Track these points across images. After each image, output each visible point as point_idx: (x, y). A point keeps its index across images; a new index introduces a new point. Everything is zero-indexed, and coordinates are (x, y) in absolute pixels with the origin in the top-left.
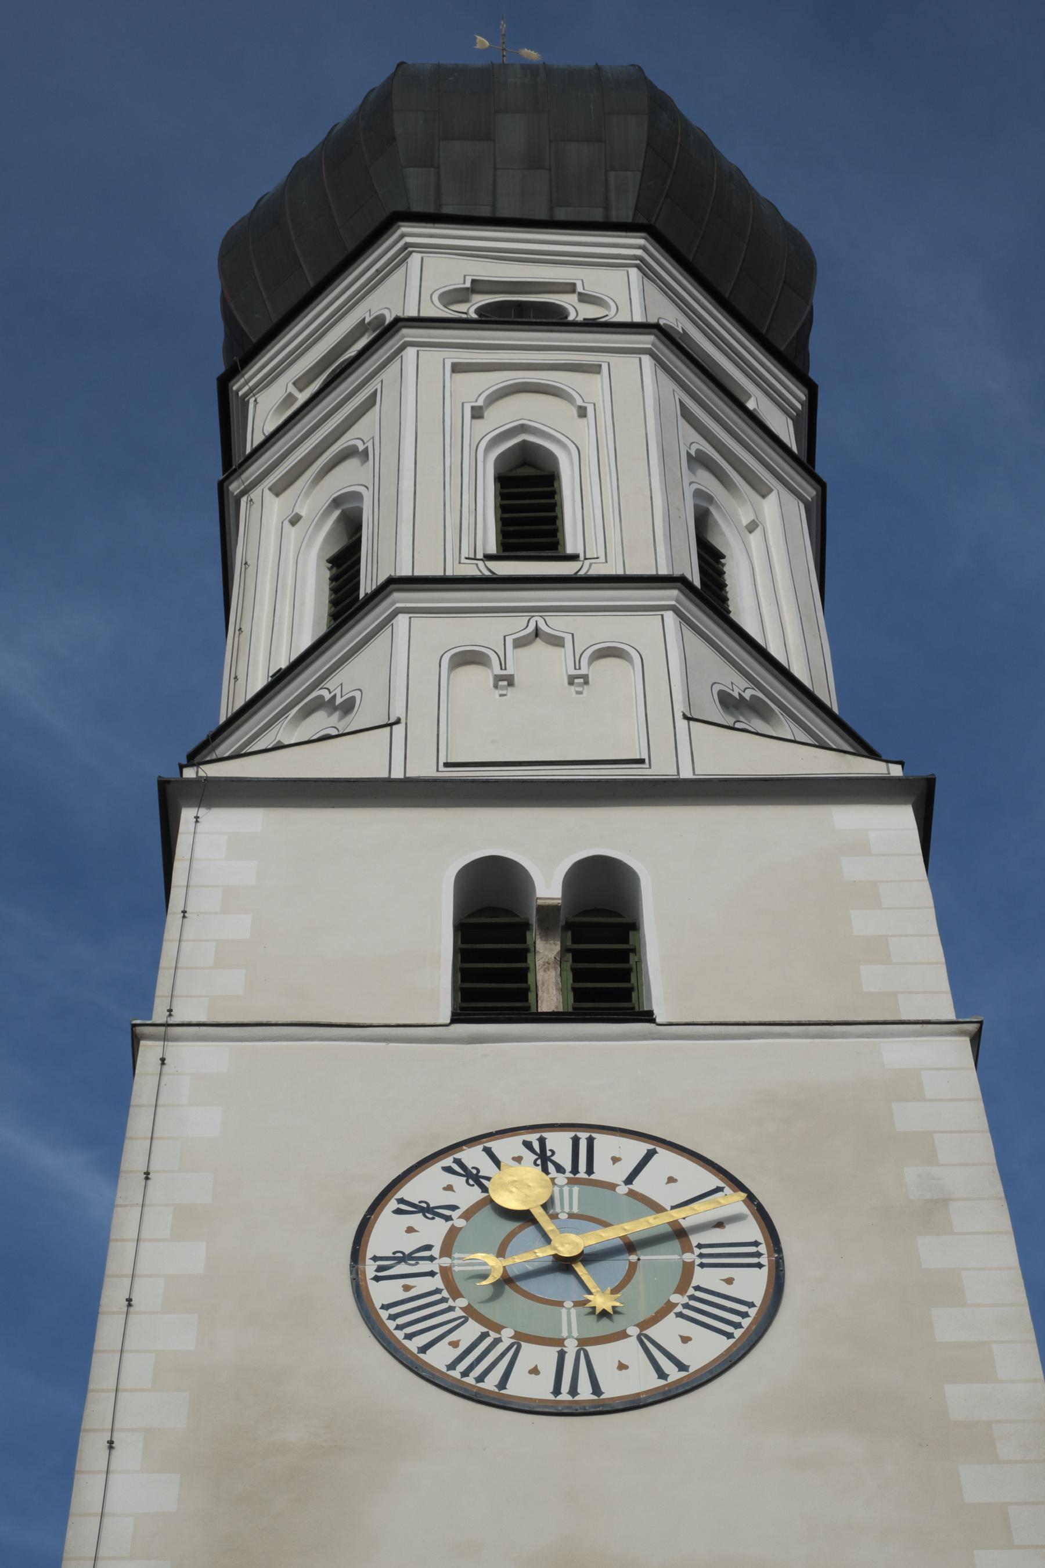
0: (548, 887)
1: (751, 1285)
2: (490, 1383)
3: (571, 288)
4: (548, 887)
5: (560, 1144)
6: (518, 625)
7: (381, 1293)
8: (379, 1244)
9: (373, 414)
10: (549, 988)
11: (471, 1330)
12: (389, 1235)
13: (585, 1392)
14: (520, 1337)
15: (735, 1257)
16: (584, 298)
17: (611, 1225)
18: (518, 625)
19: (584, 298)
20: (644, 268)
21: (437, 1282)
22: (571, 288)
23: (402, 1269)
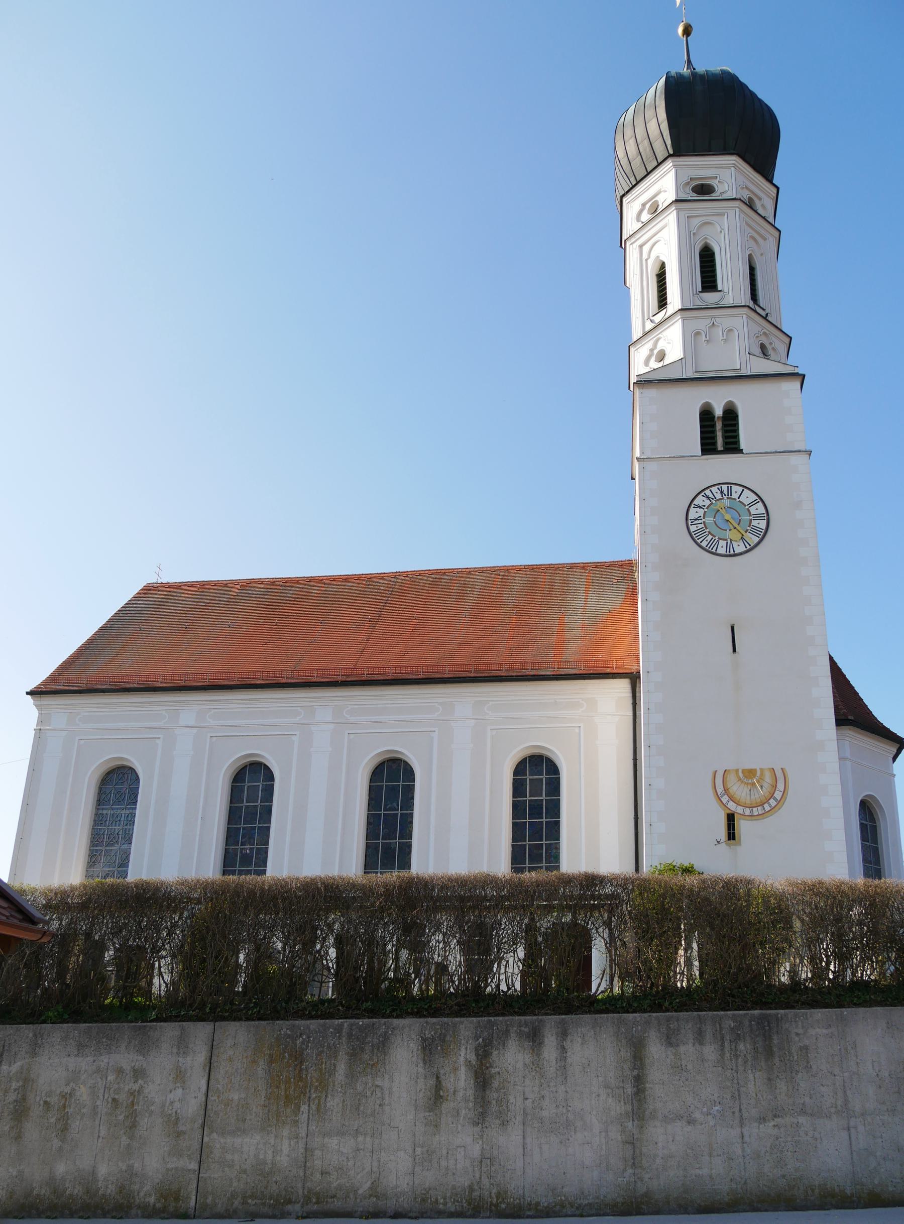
0: (719, 412)
1: (763, 524)
2: (714, 550)
3: (760, 199)
4: (719, 412)
5: (725, 487)
6: (708, 322)
7: (693, 528)
8: (691, 517)
9: (666, 230)
10: (720, 446)
11: (710, 537)
12: (693, 514)
13: (732, 552)
14: (719, 539)
15: (758, 517)
16: (763, 206)
17: (830, 655)
18: (708, 322)
19: (763, 206)
20: (735, 166)
21: (702, 525)
22: (760, 199)
23: (696, 522)
